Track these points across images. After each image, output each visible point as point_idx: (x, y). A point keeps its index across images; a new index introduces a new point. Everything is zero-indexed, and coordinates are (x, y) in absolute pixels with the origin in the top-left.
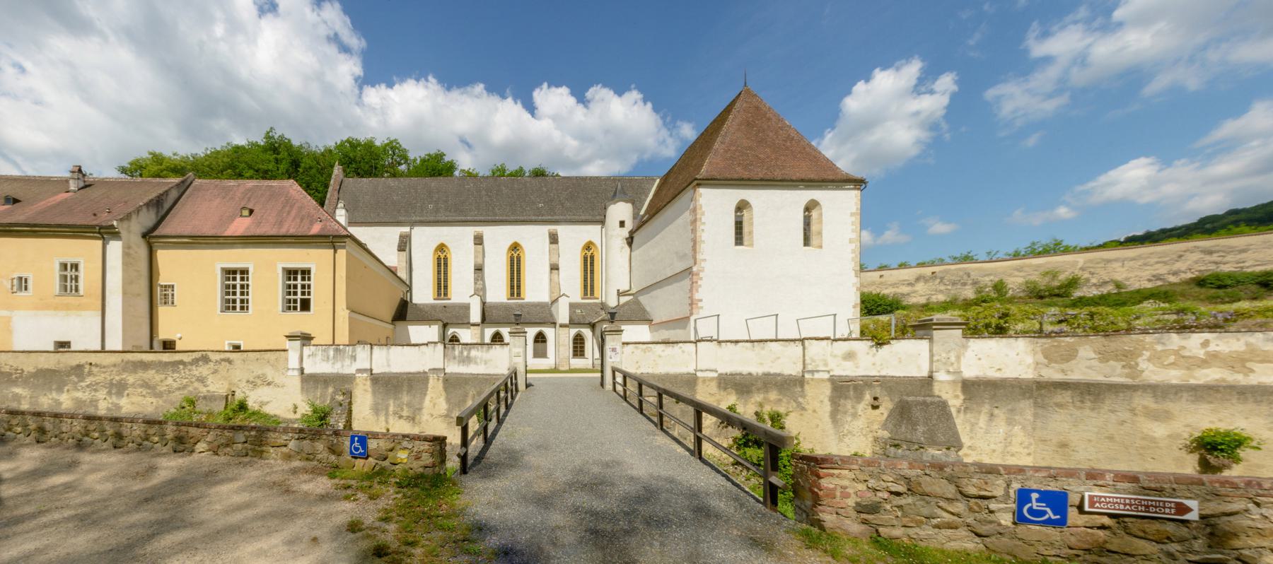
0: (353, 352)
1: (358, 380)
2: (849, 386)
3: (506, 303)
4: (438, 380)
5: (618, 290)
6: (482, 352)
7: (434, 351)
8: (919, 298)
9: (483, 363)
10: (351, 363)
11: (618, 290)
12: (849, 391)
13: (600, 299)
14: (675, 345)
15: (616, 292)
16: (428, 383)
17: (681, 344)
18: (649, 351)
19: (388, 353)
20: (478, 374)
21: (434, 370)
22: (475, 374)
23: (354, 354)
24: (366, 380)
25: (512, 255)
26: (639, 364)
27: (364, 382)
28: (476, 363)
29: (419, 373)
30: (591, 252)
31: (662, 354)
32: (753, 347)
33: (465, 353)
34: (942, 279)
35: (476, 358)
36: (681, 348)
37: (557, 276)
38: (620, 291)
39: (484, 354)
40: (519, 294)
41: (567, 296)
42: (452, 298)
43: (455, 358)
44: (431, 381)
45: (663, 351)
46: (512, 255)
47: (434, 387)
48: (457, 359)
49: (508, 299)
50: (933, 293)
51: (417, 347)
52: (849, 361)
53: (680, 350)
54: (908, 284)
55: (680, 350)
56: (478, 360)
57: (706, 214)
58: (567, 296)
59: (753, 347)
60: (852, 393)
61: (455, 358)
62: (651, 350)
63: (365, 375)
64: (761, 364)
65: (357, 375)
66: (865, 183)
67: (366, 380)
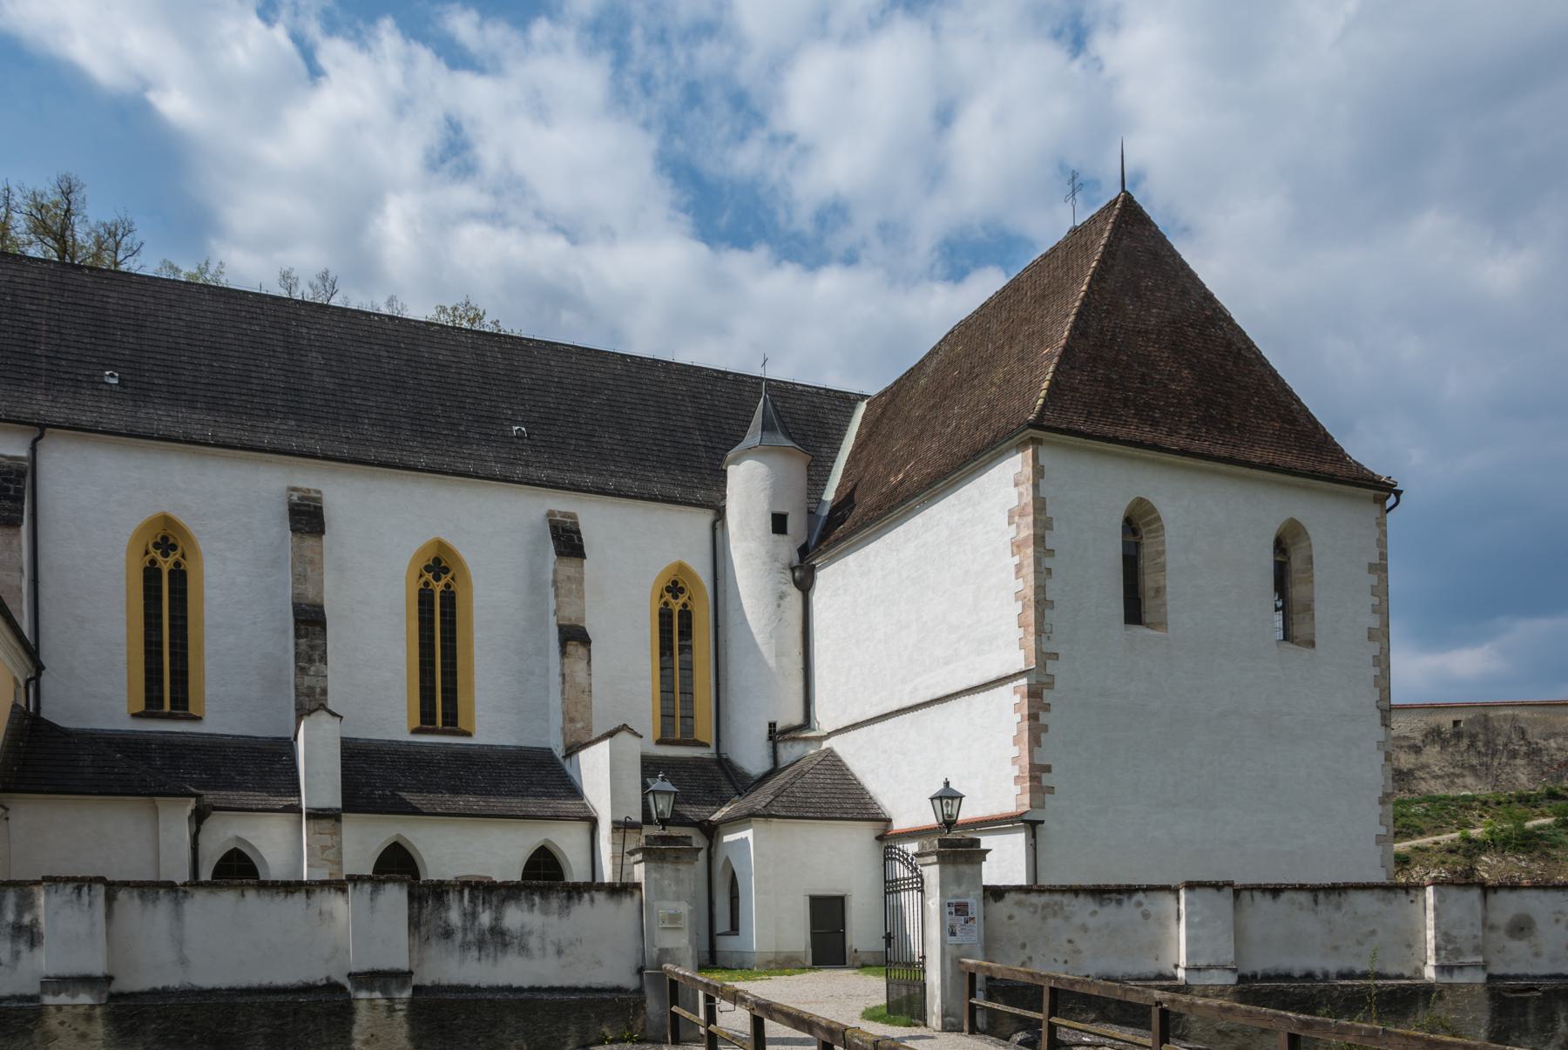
0: (20, 912)
1: (52, 1023)
2: (1527, 1000)
3: (409, 744)
4: (391, 1010)
5: (772, 725)
6: (545, 912)
7: (372, 909)
8: (1432, 782)
9: (551, 950)
10: (16, 955)
11: (772, 725)
12: (1525, 1014)
13: (713, 749)
14: (1124, 897)
15: (766, 729)
16: (352, 1023)
17: (1140, 896)
18: (1055, 914)
19: (178, 916)
20: (532, 989)
21: (369, 978)
22: (520, 990)
23: (27, 919)
24: (89, 1018)
25: (666, 604)
26: (1028, 951)
27: (82, 1027)
28: (524, 949)
29: (307, 989)
30: (681, 600)
31: (1092, 922)
32: (1316, 902)
33: (485, 918)
34: (1473, 738)
35: (524, 934)
36: (1139, 904)
37: (583, 664)
38: (778, 728)
39: (554, 919)
40: (451, 718)
41: (635, 734)
42: (208, 717)
43: (448, 934)
44: (363, 1017)
45: (1094, 913)
46: (153, 562)
47: (372, 1039)
48: (459, 936)
49: (415, 731)
50: (1458, 771)
51: (299, 898)
52: (1520, 939)
53: (1138, 912)
54: (1410, 747)
55: (1138, 912)
56: (533, 942)
57: (1055, 525)
58: (635, 734)
59: (1316, 902)
60: (1531, 1018)
61: (448, 934)
62: (1062, 908)
63: (85, 999)
64: (1336, 948)
65: (49, 1000)
66: (1398, 493)
67: (89, 1018)
